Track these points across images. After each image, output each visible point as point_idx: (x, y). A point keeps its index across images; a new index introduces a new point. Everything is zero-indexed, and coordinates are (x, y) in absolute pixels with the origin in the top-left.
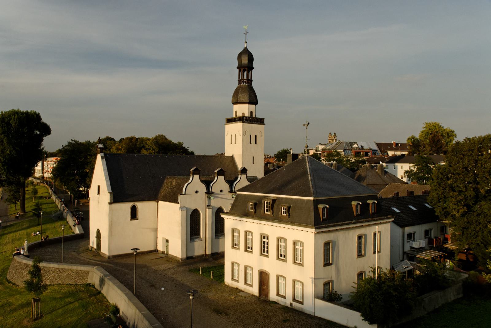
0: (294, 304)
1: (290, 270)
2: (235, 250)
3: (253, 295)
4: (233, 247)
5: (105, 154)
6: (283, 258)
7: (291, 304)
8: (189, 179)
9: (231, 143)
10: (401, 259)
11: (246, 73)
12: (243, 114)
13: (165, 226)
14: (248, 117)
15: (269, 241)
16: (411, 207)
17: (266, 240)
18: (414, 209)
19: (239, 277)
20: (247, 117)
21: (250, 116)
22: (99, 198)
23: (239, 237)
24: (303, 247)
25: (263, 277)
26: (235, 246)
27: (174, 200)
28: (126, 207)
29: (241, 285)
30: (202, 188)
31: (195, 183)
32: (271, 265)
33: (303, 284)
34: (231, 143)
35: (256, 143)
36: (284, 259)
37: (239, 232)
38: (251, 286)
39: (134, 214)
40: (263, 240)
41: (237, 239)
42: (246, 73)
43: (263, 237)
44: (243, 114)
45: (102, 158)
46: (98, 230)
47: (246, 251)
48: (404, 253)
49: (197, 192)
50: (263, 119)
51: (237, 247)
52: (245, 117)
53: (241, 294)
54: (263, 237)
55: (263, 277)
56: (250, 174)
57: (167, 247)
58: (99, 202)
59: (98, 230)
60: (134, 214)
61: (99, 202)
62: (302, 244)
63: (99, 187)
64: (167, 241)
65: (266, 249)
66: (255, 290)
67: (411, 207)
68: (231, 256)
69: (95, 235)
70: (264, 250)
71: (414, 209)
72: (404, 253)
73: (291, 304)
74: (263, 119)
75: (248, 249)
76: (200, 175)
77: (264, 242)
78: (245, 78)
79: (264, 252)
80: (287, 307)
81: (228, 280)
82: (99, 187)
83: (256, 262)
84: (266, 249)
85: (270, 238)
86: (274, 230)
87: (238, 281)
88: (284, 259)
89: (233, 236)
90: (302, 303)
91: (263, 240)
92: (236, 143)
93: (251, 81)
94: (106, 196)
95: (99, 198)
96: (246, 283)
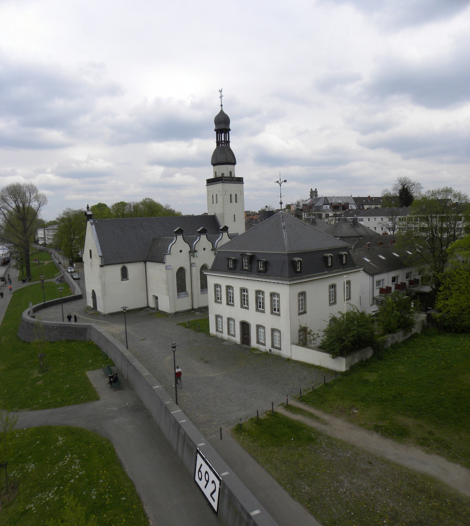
0: (273, 350)
1: (267, 320)
2: (259, 314)
3: (236, 344)
4: (216, 301)
5: (94, 221)
6: (276, 312)
7: (270, 350)
8: (173, 239)
9: (213, 203)
10: (371, 304)
11: (223, 134)
12: (223, 174)
13: (156, 284)
14: (228, 177)
15: (264, 297)
16: (381, 257)
17: (245, 294)
18: (383, 258)
19: (222, 328)
20: (226, 177)
21: (229, 176)
22: (91, 262)
23: (221, 291)
24: (279, 298)
25: (245, 326)
26: (218, 299)
27: (161, 261)
28: (116, 270)
29: (225, 335)
30: (186, 248)
31: (179, 245)
32: (252, 317)
33: (280, 332)
34: (213, 203)
35: (236, 202)
36: (278, 313)
37: (220, 288)
38: (234, 336)
39: (124, 275)
40: (244, 293)
41: (219, 293)
42: (223, 134)
43: (258, 292)
44: (223, 174)
45: (92, 224)
46: (93, 290)
47: (228, 304)
48: (374, 298)
49: (181, 251)
50: (242, 178)
51: (219, 301)
52: (225, 177)
53: (225, 343)
54: (243, 290)
55: (245, 326)
56: (231, 231)
57: (157, 303)
58: (91, 265)
59: (93, 290)
60: (124, 275)
61: (91, 265)
62: (278, 295)
63: (91, 251)
64: (157, 298)
65: (246, 302)
66: (237, 339)
67: (381, 257)
68: (215, 309)
69: (91, 296)
70: (260, 306)
71: (383, 258)
72: (374, 298)
73: (270, 350)
74: (242, 178)
75: (230, 302)
76: (183, 235)
77: (244, 295)
78: (223, 139)
79: (244, 304)
80: (267, 352)
81: (213, 330)
82: (91, 251)
83: (238, 314)
84: (246, 302)
85: (249, 292)
86: (253, 285)
87: (222, 332)
88: (278, 313)
89: (216, 291)
90: (280, 349)
91: (244, 293)
92: (217, 203)
93: (228, 142)
94: (97, 261)
95: (91, 262)
96: (229, 333)
